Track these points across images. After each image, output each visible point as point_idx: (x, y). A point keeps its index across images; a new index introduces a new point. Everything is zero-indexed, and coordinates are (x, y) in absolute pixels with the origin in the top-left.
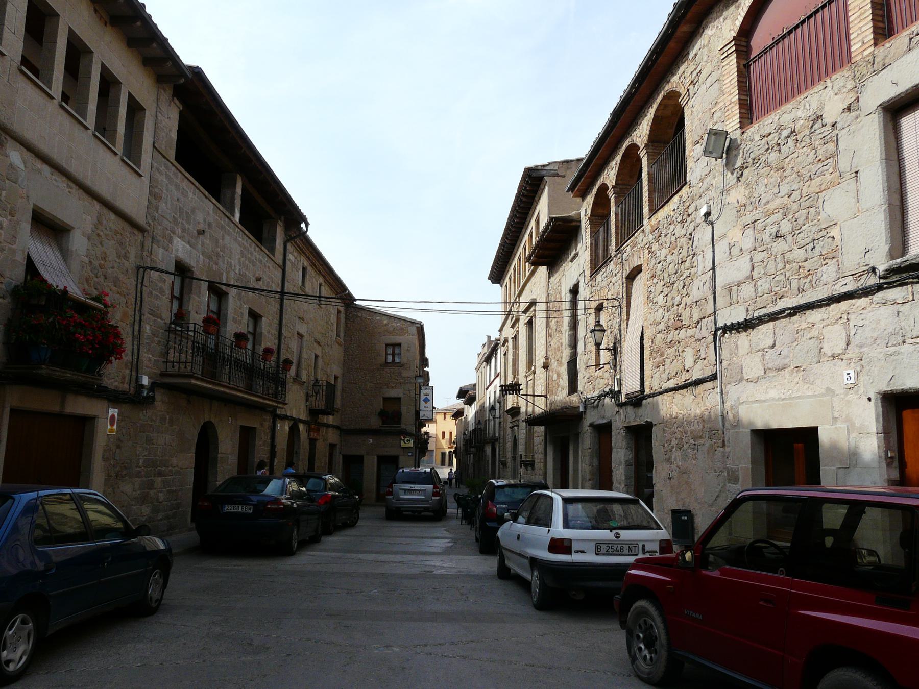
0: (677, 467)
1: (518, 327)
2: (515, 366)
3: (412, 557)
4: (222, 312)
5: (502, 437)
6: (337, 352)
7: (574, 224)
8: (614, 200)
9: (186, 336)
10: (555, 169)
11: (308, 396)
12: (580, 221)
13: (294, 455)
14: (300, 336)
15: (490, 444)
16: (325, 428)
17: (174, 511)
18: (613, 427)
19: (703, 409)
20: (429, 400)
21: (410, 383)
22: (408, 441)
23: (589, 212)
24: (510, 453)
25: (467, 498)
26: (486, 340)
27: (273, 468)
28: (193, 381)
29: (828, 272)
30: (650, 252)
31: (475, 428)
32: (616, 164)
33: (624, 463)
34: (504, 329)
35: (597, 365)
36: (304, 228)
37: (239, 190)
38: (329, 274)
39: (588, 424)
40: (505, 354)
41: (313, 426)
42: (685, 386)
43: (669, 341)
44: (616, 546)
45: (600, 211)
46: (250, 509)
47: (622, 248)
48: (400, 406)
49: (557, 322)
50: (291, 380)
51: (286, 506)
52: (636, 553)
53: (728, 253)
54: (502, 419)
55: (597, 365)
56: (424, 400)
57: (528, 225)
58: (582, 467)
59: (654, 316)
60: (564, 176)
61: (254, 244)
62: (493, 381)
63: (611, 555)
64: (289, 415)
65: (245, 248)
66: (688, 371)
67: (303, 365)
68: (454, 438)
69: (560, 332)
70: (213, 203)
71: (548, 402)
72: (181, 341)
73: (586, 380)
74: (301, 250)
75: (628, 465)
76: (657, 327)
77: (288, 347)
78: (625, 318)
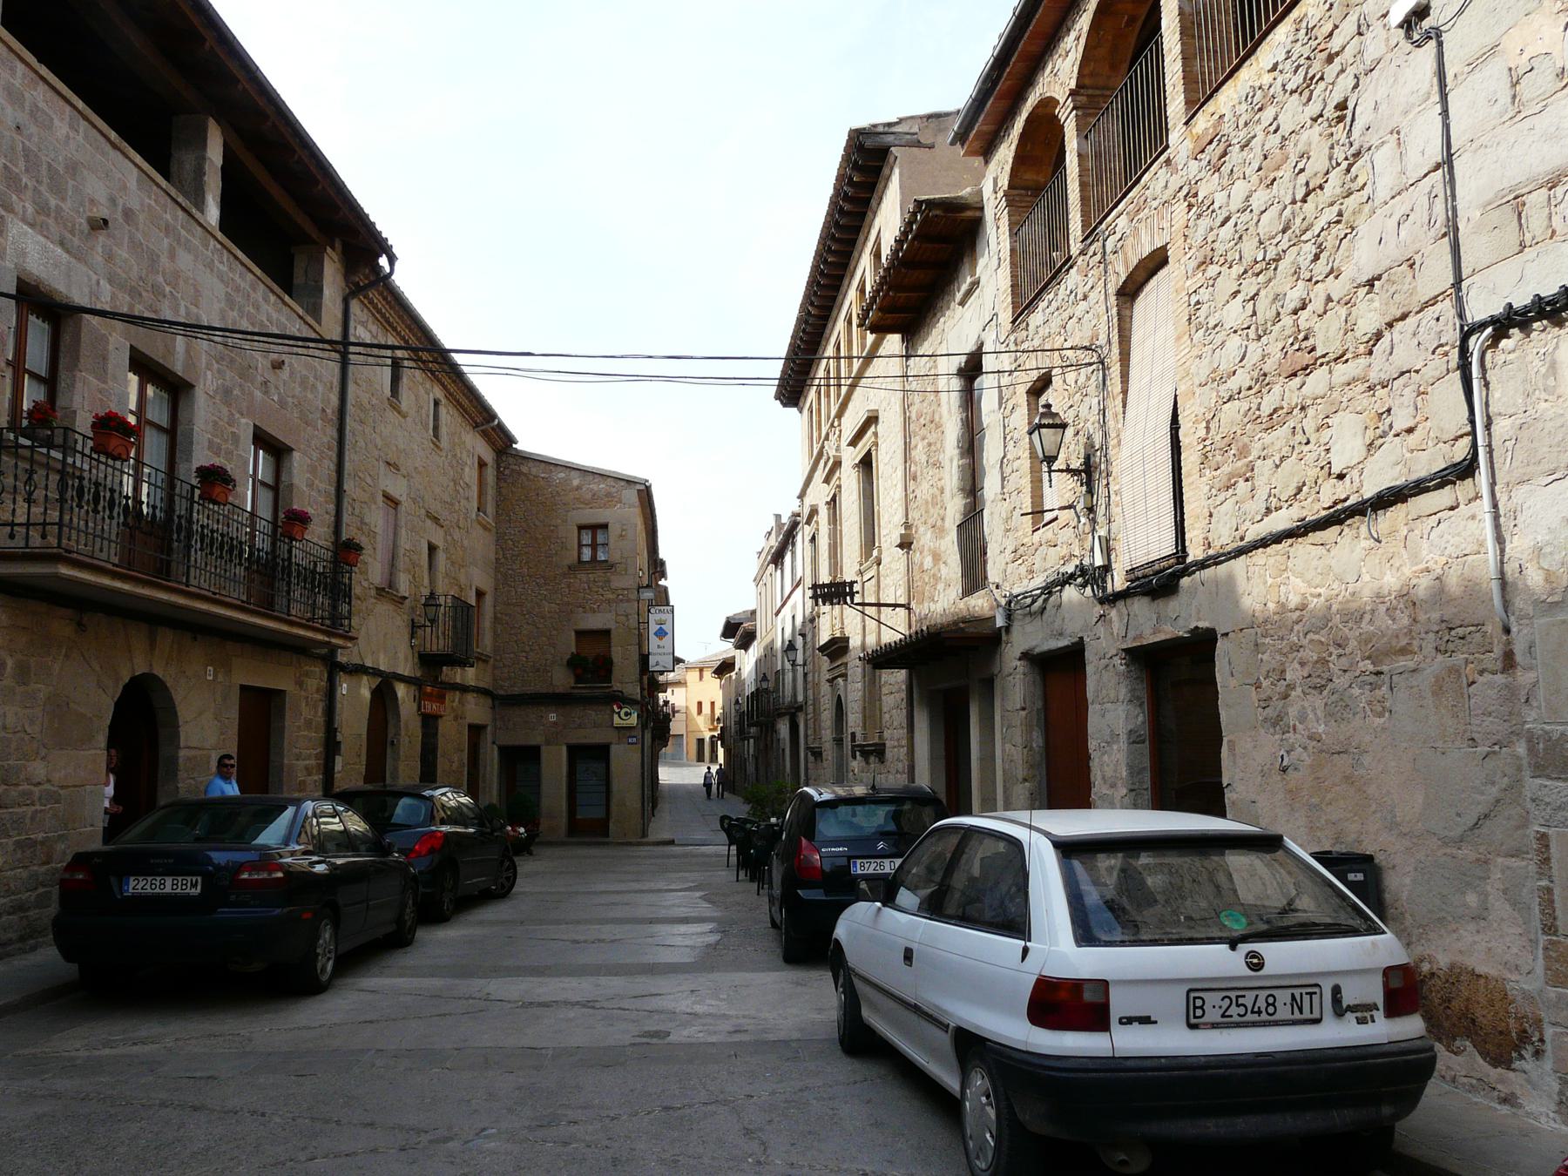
0: (1310, 738)
1: (839, 478)
2: (836, 554)
3: (616, 984)
4: (180, 429)
5: (810, 702)
6: (479, 544)
7: (969, 214)
8: (1074, 124)
9: (44, 460)
10: (912, 131)
11: (414, 627)
12: (982, 209)
13: (389, 751)
14: (392, 502)
15: (788, 717)
16: (458, 693)
17: (41, 890)
18: (1089, 655)
19: (1407, 571)
20: (666, 634)
21: (628, 601)
22: (626, 714)
23: (1004, 182)
24: (829, 732)
25: (748, 826)
26: (773, 523)
27: (333, 778)
28: (65, 570)
30: (1190, 206)
31: (757, 690)
32: (1078, 39)
33: (1123, 738)
34: (809, 491)
35: (1037, 512)
36: (387, 269)
37: (215, 154)
38: (454, 382)
39: (1018, 655)
40: (813, 539)
41: (429, 689)
42: (1337, 517)
43: (1266, 410)
44: (1250, 995)
45: (1029, 176)
46: (194, 885)
47: (1103, 226)
48: (610, 647)
49: (930, 445)
50: (373, 592)
51: (290, 874)
52: (1316, 1015)
53: (1505, 98)
54: (809, 667)
55: (1037, 512)
56: (656, 634)
57: (855, 268)
58: (1003, 751)
59: (1211, 362)
60: (931, 147)
61: (262, 286)
62: (789, 597)
63: (1238, 1025)
64: (368, 664)
65: (238, 289)
66: (1341, 477)
67: (402, 563)
68: (718, 712)
69: (938, 465)
70: (136, 165)
71: (913, 619)
72: (31, 473)
73: (1008, 556)
74: (387, 321)
75: (1134, 742)
76: (1223, 387)
77: (362, 522)
78: (1118, 388)
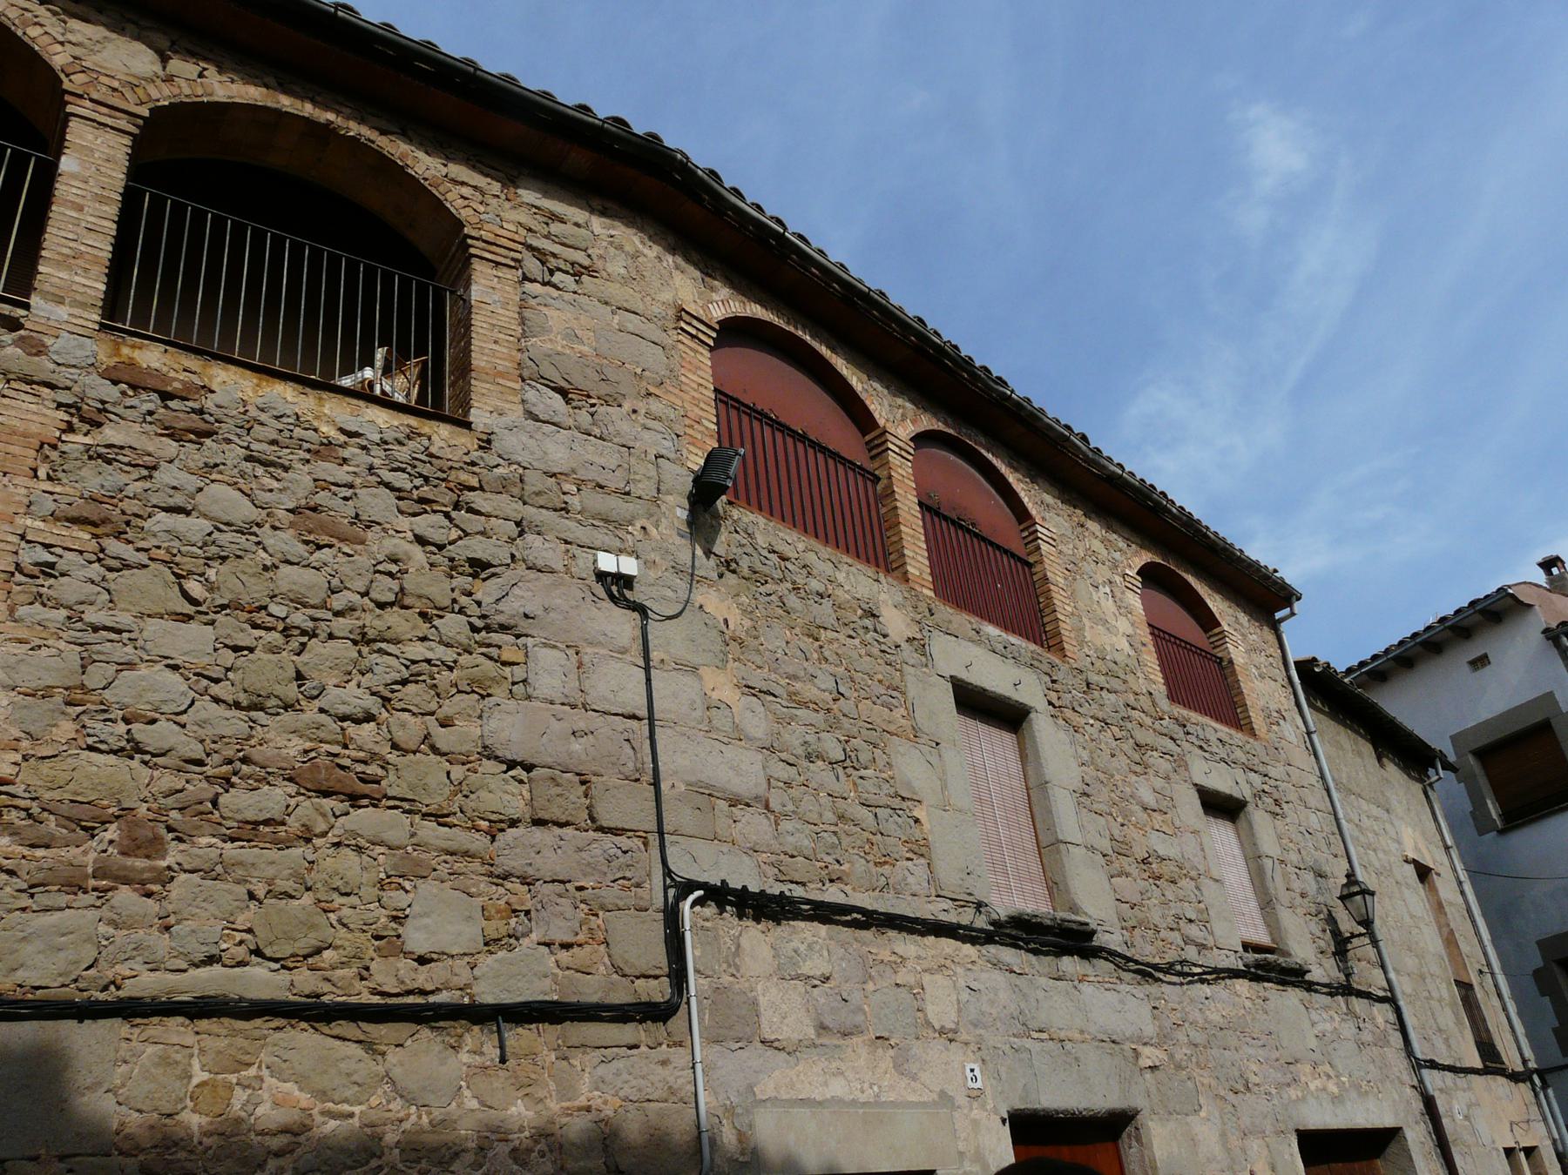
29: (914, 874)
